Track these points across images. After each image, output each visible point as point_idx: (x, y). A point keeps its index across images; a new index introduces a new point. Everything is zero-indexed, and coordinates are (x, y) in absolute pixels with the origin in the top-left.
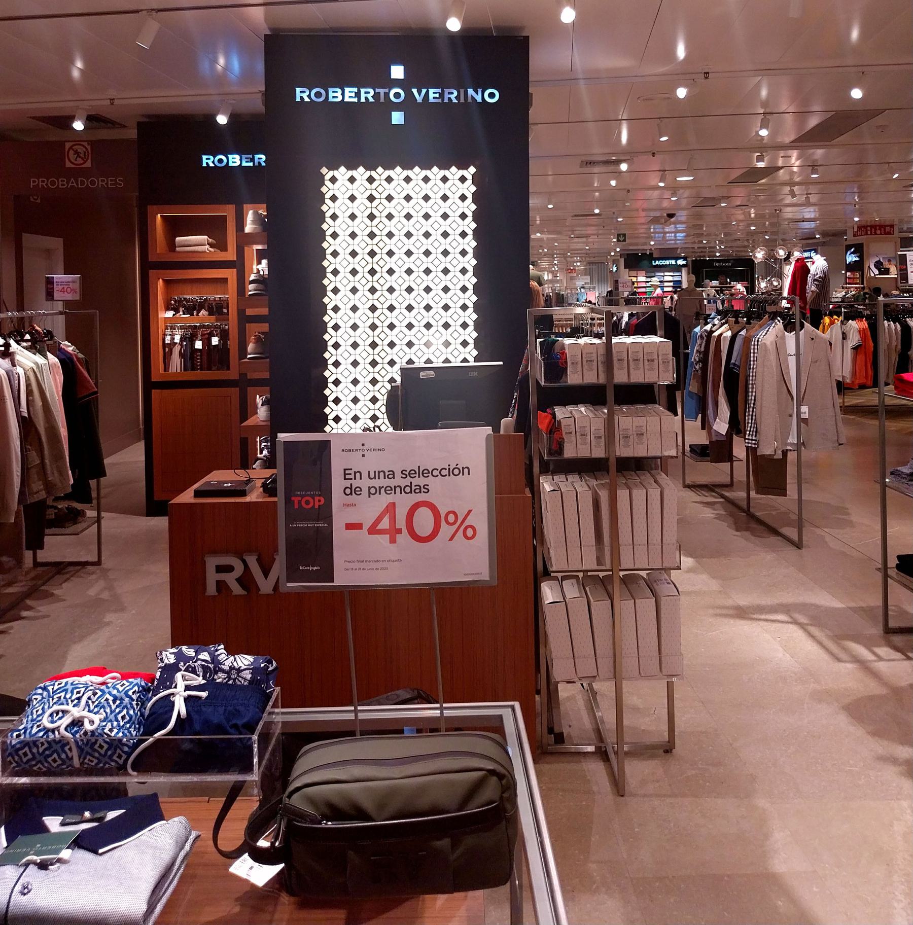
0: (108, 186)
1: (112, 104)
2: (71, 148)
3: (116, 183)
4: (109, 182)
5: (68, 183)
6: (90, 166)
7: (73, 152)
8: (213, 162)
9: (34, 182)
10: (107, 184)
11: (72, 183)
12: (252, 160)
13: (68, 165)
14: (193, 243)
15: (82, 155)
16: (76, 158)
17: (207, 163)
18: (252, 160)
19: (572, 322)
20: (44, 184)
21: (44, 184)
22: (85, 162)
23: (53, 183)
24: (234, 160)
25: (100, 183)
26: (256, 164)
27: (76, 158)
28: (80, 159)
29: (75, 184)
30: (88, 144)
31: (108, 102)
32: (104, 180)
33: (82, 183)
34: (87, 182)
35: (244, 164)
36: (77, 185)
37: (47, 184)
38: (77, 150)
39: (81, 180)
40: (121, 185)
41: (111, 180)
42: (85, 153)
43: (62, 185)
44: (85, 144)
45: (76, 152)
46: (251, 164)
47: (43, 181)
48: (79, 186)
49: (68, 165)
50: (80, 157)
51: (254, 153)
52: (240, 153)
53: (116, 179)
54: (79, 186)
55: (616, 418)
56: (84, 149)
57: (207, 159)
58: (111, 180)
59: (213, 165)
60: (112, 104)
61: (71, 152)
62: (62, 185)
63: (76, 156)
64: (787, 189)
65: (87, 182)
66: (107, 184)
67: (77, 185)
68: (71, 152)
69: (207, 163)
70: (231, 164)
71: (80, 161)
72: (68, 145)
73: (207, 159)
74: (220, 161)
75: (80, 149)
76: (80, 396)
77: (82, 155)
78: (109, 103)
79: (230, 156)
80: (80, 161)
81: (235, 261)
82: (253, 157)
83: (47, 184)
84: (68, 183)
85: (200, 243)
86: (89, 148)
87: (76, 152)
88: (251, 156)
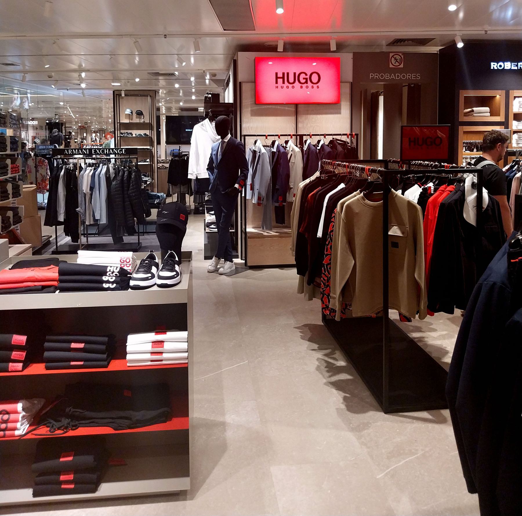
0: (412, 78)
1: (486, 33)
2: (393, 56)
3: (416, 77)
4: (413, 76)
5: (390, 76)
6: (390, 67)
7: (394, 59)
8: (497, 66)
9: (372, 75)
10: (411, 77)
11: (393, 76)
12: (517, 66)
13: (391, 66)
14: (484, 112)
15: (399, 61)
16: (395, 62)
17: (493, 67)
18: (517, 66)
19: (8, 148)
20: (377, 77)
21: (377, 77)
22: (400, 64)
23: (404, 76)
24: (507, 66)
25: (408, 77)
26: (519, 68)
27: (395, 62)
28: (398, 63)
29: (394, 77)
30: (402, 55)
31: (484, 32)
32: (410, 75)
33: (404, 76)
34: (401, 77)
35: (513, 68)
36: (395, 78)
37: (379, 77)
38: (396, 58)
39: (397, 75)
40: (419, 78)
41: (414, 75)
42: (400, 59)
43: (387, 77)
44: (401, 54)
45: (396, 59)
46: (516, 68)
47: (377, 75)
48: (396, 78)
49: (391, 66)
50: (397, 62)
51: (518, 62)
52: (512, 62)
53: (416, 74)
54: (396, 78)
55: (46, 201)
56: (400, 57)
57: (494, 65)
58: (414, 75)
59: (497, 68)
60: (486, 33)
61: (393, 59)
62: (387, 77)
63: (395, 61)
64: (76, 75)
65: (401, 77)
66: (411, 77)
67: (395, 78)
68: (393, 59)
69: (493, 67)
70: (506, 68)
71: (397, 64)
72: (391, 55)
73: (494, 65)
74: (500, 66)
75: (398, 57)
76: (173, 187)
77: (399, 61)
78: (485, 33)
79: (506, 63)
80: (397, 64)
81: (504, 122)
82: (518, 64)
83: (379, 77)
84: (390, 76)
85: (485, 111)
86: (402, 56)
87: (396, 59)
88: (516, 64)
